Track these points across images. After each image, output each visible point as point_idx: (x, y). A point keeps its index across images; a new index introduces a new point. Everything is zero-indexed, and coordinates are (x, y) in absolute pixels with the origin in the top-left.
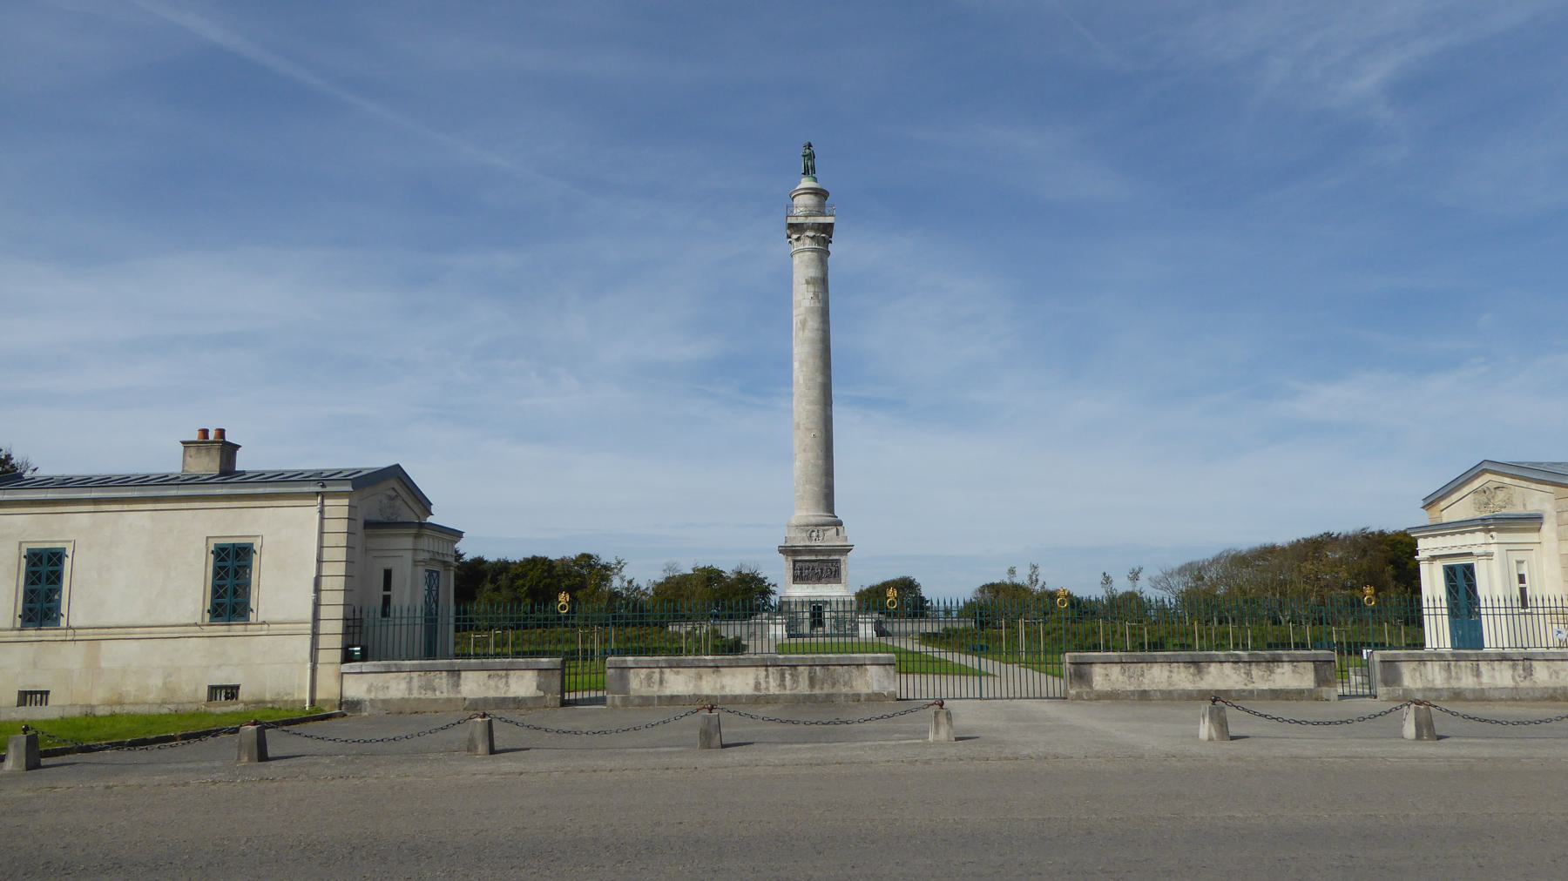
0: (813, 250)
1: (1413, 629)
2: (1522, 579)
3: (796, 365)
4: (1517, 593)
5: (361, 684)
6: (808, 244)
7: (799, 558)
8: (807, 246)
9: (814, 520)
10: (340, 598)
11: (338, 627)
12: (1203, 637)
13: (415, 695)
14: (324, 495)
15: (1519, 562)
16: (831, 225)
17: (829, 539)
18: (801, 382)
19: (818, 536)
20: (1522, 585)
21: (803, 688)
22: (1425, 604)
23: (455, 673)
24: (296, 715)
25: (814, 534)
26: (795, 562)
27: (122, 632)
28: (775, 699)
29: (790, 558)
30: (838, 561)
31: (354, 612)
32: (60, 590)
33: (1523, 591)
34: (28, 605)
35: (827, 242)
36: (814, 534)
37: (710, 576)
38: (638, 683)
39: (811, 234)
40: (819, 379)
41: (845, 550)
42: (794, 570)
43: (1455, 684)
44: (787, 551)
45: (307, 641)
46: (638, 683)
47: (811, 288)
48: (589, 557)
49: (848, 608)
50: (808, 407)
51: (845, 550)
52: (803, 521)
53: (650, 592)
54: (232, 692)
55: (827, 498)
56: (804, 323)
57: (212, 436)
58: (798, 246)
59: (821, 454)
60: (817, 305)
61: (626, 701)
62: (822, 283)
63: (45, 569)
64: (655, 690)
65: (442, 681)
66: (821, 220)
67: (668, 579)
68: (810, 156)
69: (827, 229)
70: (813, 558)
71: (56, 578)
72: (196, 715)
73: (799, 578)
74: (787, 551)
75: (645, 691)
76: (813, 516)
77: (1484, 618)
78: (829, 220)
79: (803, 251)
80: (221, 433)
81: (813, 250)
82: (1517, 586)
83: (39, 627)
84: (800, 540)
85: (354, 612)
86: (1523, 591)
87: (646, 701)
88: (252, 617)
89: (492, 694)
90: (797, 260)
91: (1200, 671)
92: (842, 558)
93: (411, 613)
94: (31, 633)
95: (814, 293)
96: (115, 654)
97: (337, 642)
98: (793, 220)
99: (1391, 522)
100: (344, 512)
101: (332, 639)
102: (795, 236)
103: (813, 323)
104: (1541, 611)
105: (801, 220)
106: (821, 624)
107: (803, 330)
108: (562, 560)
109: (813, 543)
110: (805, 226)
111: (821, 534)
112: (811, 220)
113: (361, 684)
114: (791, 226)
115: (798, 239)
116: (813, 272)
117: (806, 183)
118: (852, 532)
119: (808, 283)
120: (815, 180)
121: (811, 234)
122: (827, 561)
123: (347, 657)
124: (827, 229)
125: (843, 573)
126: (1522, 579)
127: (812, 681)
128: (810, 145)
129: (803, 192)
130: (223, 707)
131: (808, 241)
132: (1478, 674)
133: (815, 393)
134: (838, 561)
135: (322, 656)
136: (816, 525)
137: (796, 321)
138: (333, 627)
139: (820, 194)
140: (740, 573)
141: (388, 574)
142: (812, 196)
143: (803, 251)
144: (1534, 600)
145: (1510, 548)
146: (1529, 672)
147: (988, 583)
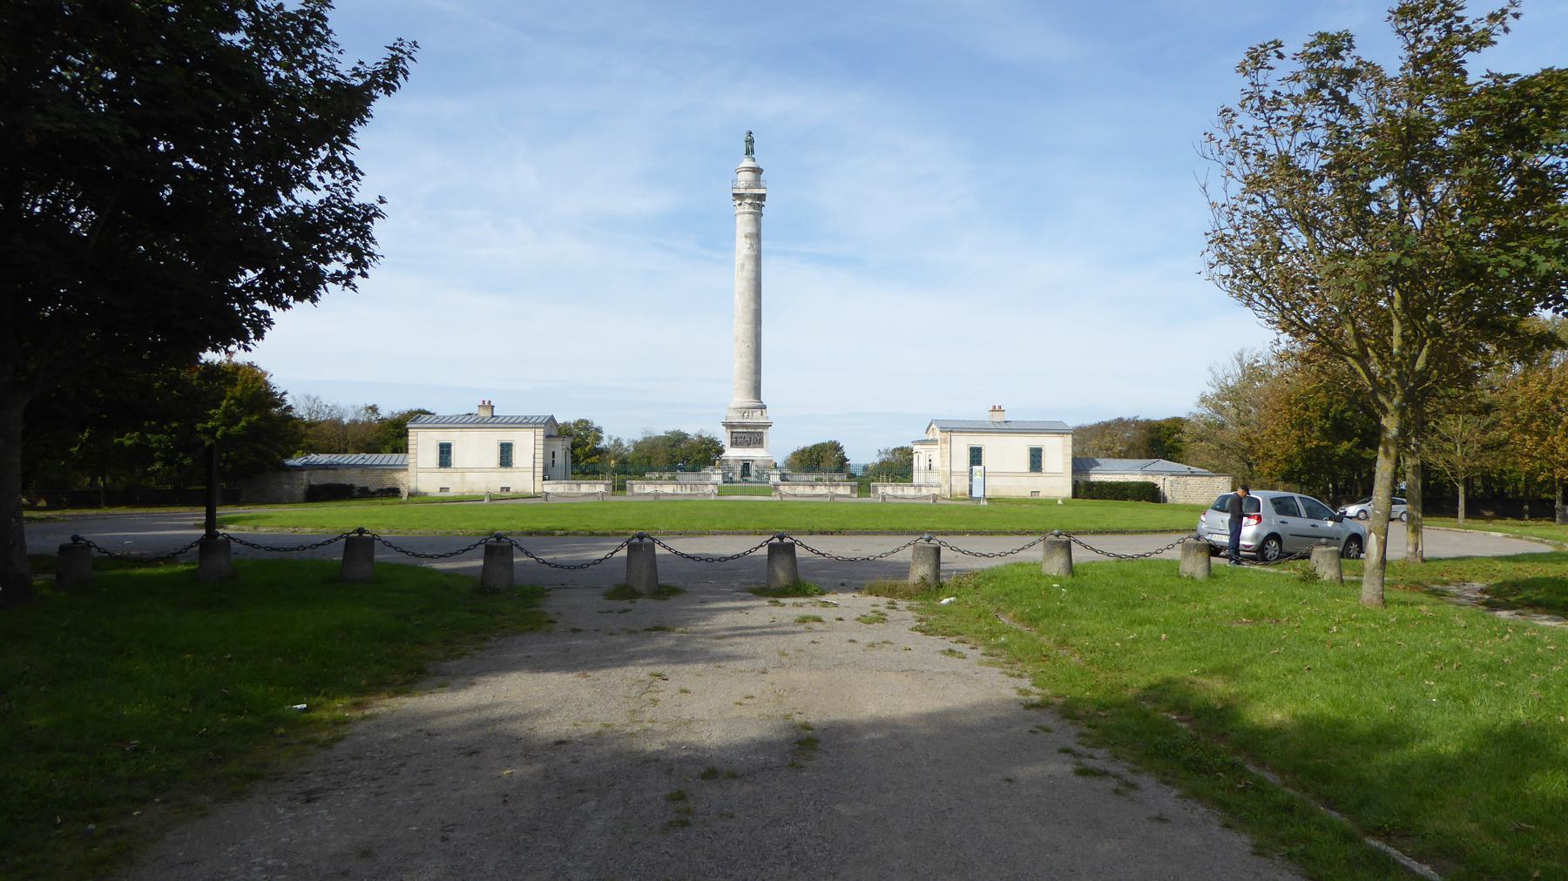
0: (750, 213)
1: (1076, 482)
2: (930, 461)
3: (737, 296)
5: (549, 487)
6: (747, 208)
7: (735, 430)
8: (746, 210)
9: (746, 405)
10: (542, 460)
11: (541, 470)
13: (566, 491)
14: (535, 428)
15: (930, 455)
16: (764, 195)
17: (756, 417)
18: (740, 308)
21: (688, 491)
23: (579, 485)
24: (529, 495)
26: (732, 433)
27: (471, 470)
28: (680, 494)
29: (729, 430)
30: (762, 433)
32: (450, 456)
33: (930, 465)
35: (760, 207)
37: (677, 439)
38: (636, 489)
39: (749, 201)
40: (753, 306)
41: (767, 426)
43: (896, 494)
44: (729, 426)
45: (532, 473)
46: (636, 489)
47: (748, 241)
48: (587, 422)
50: (744, 326)
51: (767, 426)
52: (739, 406)
53: (632, 449)
54: (508, 489)
55: (756, 390)
56: (743, 266)
57: (486, 404)
58: (740, 209)
59: (752, 359)
60: (753, 253)
61: (633, 495)
62: (756, 237)
63: (445, 449)
64: (642, 491)
65: (575, 487)
66: (757, 191)
67: (645, 438)
68: (750, 142)
69: (761, 197)
70: (745, 430)
71: (449, 452)
72: (498, 495)
73: (734, 444)
74: (729, 426)
75: (639, 492)
78: (762, 191)
79: (744, 213)
80: (490, 402)
81: (750, 213)
82: (928, 463)
83: (445, 467)
84: (736, 418)
86: (930, 465)
87: (639, 495)
88: (513, 466)
89: (591, 492)
90: (739, 219)
91: (814, 488)
92: (765, 431)
94: (442, 469)
95: (751, 244)
96: (469, 477)
97: (541, 474)
98: (737, 191)
99: (905, 443)
100: (542, 433)
101: (539, 475)
102: (738, 202)
103: (749, 266)
105: (742, 191)
106: (749, 475)
107: (742, 271)
108: (565, 423)
111: (750, 414)
112: (749, 191)
113: (549, 487)
114: (735, 195)
115: (740, 204)
116: (750, 229)
117: (747, 163)
118: (771, 414)
119: (746, 237)
120: (754, 160)
121: (749, 201)
122: (752, 433)
123: (544, 479)
124: (761, 197)
125: (765, 441)
126: (930, 461)
127: (691, 489)
128: (751, 133)
130: (505, 494)
131: (747, 206)
132: (903, 490)
133: (749, 317)
134: (762, 433)
135: (536, 479)
136: (748, 408)
137: (738, 263)
138: (539, 470)
139: (757, 171)
140: (700, 436)
141: (554, 453)
142: (751, 173)
143: (744, 213)
145: (927, 450)
146: (920, 490)
147: (899, 447)
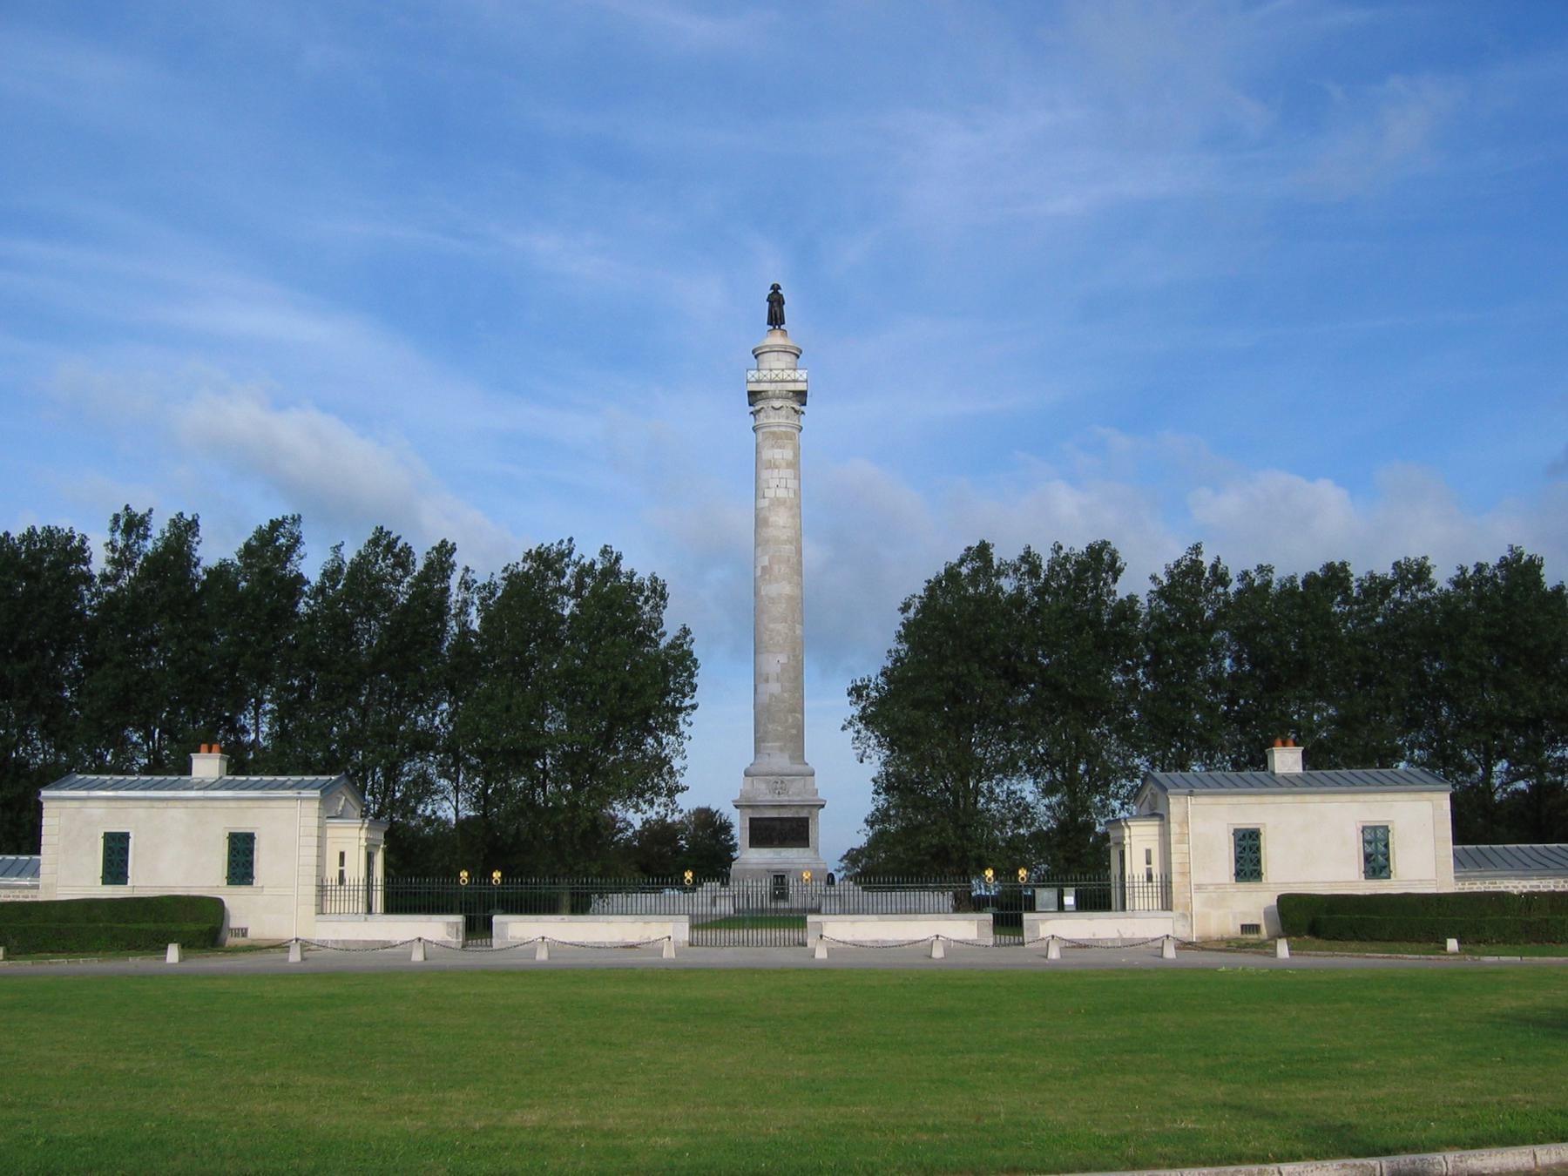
86: (341, 873)
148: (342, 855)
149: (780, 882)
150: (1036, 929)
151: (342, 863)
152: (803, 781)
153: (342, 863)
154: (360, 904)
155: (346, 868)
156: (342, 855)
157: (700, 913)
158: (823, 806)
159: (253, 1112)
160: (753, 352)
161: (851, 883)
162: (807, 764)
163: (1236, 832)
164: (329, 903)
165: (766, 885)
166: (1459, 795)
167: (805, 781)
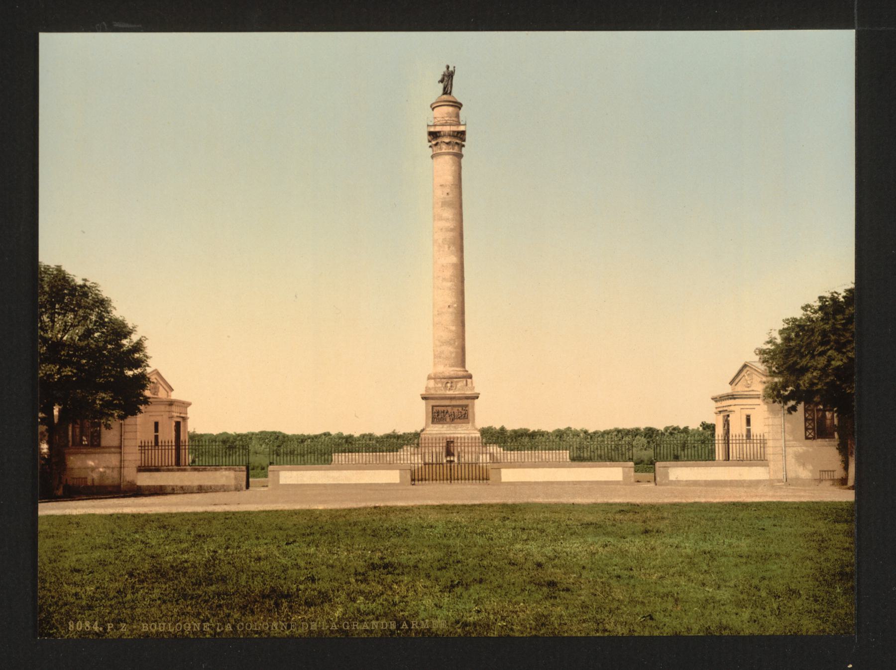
4: (745, 433)
12: (206, 468)
17: (459, 390)
19: (451, 386)
20: (748, 427)
22: (716, 438)
25: (449, 385)
31: (141, 443)
34: (280, 438)
36: (449, 385)
42: (433, 413)
49: (477, 441)
76: (460, 371)
77: (717, 445)
85: (141, 443)
93: (170, 444)
104: (167, 447)
109: (448, 392)
110: (442, 133)
111: (454, 384)
112: (447, 129)
118: (478, 385)
129: (451, 104)
134: (467, 406)
144: (755, 436)
148: (156, 424)
149: (449, 447)
150: (666, 475)
151: (156, 430)
152: (465, 382)
153: (156, 430)
154: (183, 459)
155: (160, 434)
156: (156, 424)
157: (484, 455)
158: (477, 398)
159: (285, 569)
160: (431, 107)
161: (502, 449)
162: (467, 371)
163: (715, 425)
164: (183, 451)
165: (441, 449)
166: (540, 447)
167: (467, 381)
